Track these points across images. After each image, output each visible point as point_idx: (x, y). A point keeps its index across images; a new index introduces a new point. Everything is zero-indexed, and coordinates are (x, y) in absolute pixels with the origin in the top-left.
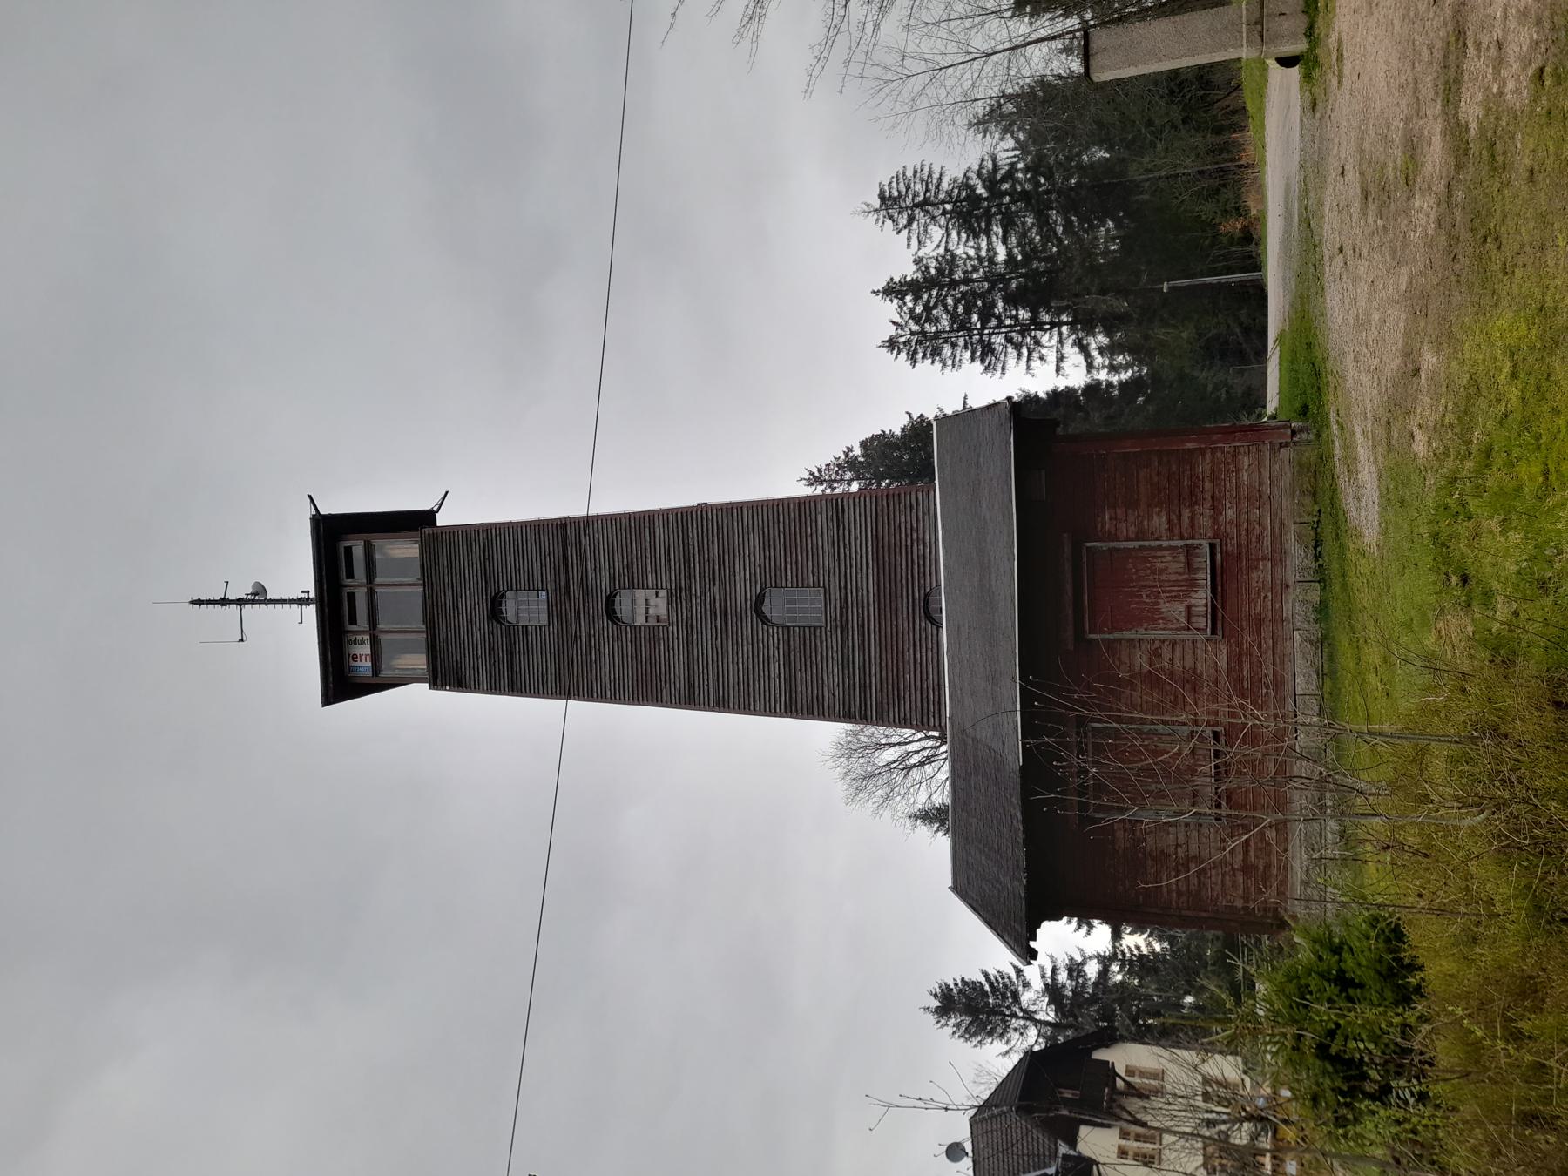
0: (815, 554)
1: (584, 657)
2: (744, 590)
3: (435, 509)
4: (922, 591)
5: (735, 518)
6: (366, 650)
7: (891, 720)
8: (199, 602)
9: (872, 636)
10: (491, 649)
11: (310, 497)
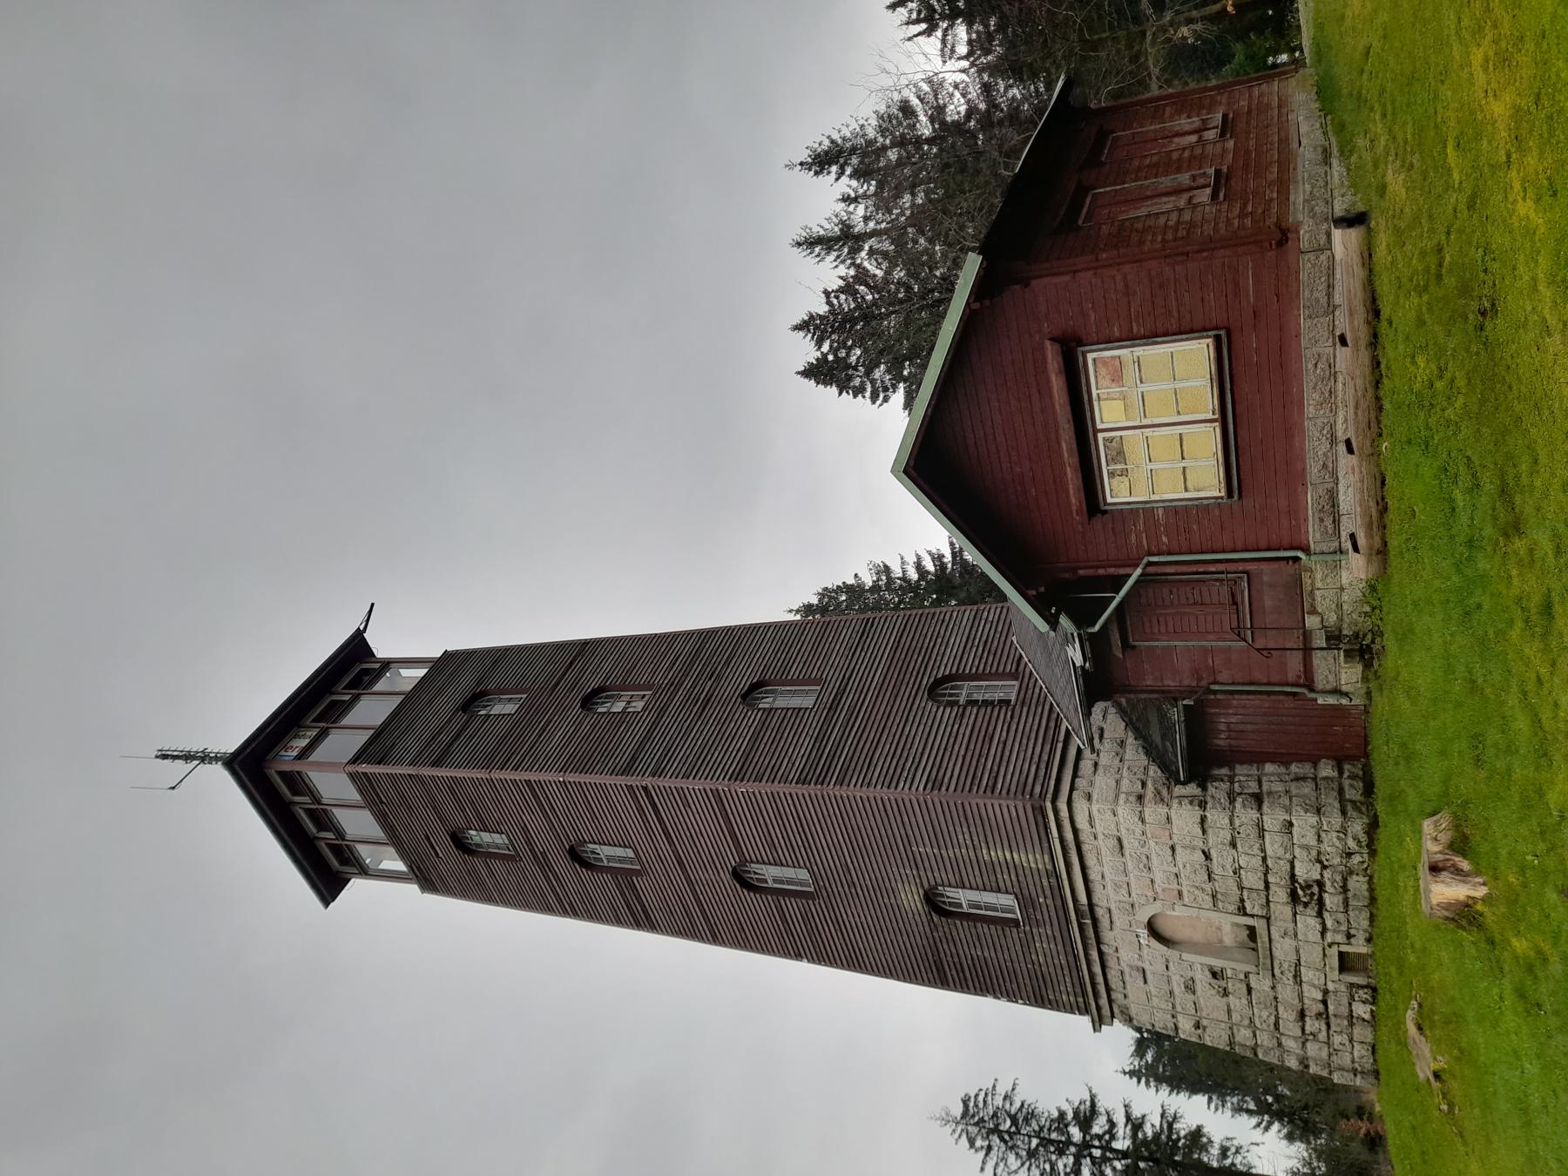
3: (362, 628)
11: (373, 605)
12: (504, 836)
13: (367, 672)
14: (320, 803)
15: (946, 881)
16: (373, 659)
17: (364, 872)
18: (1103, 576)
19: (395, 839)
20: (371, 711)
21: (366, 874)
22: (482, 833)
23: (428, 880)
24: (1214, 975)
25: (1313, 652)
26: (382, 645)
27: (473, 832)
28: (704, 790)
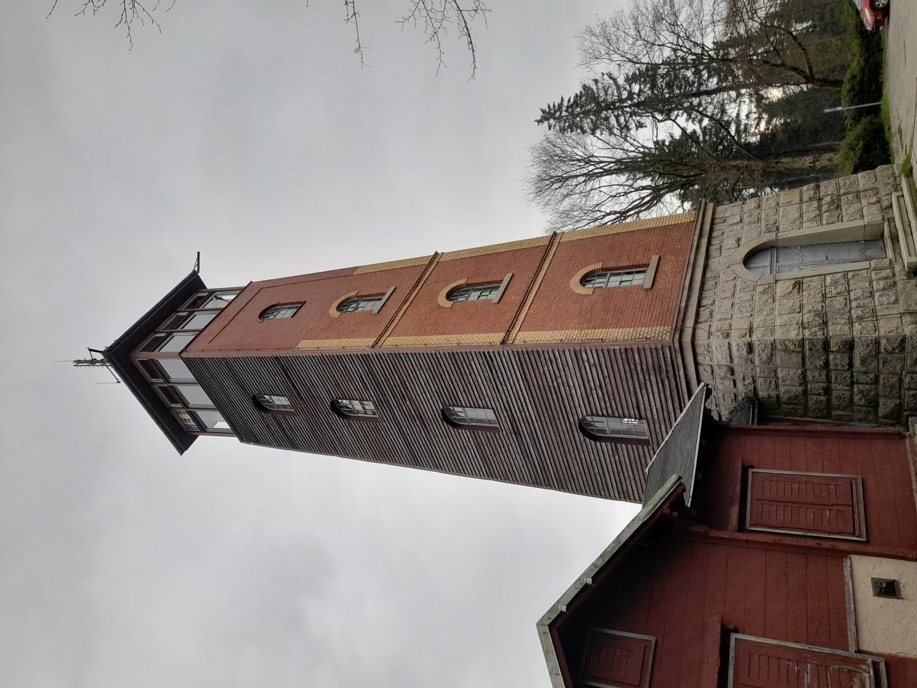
2: (431, 407)
3: (196, 269)
4: (576, 417)
5: (404, 360)
6: (187, 417)
7: (578, 488)
8: (79, 362)
9: (542, 441)
11: (199, 253)
12: (286, 397)
14: (169, 382)
16: (205, 290)
18: (848, 640)
19: (221, 406)
21: (205, 432)
23: (246, 434)
24: (843, 67)
26: (210, 283)
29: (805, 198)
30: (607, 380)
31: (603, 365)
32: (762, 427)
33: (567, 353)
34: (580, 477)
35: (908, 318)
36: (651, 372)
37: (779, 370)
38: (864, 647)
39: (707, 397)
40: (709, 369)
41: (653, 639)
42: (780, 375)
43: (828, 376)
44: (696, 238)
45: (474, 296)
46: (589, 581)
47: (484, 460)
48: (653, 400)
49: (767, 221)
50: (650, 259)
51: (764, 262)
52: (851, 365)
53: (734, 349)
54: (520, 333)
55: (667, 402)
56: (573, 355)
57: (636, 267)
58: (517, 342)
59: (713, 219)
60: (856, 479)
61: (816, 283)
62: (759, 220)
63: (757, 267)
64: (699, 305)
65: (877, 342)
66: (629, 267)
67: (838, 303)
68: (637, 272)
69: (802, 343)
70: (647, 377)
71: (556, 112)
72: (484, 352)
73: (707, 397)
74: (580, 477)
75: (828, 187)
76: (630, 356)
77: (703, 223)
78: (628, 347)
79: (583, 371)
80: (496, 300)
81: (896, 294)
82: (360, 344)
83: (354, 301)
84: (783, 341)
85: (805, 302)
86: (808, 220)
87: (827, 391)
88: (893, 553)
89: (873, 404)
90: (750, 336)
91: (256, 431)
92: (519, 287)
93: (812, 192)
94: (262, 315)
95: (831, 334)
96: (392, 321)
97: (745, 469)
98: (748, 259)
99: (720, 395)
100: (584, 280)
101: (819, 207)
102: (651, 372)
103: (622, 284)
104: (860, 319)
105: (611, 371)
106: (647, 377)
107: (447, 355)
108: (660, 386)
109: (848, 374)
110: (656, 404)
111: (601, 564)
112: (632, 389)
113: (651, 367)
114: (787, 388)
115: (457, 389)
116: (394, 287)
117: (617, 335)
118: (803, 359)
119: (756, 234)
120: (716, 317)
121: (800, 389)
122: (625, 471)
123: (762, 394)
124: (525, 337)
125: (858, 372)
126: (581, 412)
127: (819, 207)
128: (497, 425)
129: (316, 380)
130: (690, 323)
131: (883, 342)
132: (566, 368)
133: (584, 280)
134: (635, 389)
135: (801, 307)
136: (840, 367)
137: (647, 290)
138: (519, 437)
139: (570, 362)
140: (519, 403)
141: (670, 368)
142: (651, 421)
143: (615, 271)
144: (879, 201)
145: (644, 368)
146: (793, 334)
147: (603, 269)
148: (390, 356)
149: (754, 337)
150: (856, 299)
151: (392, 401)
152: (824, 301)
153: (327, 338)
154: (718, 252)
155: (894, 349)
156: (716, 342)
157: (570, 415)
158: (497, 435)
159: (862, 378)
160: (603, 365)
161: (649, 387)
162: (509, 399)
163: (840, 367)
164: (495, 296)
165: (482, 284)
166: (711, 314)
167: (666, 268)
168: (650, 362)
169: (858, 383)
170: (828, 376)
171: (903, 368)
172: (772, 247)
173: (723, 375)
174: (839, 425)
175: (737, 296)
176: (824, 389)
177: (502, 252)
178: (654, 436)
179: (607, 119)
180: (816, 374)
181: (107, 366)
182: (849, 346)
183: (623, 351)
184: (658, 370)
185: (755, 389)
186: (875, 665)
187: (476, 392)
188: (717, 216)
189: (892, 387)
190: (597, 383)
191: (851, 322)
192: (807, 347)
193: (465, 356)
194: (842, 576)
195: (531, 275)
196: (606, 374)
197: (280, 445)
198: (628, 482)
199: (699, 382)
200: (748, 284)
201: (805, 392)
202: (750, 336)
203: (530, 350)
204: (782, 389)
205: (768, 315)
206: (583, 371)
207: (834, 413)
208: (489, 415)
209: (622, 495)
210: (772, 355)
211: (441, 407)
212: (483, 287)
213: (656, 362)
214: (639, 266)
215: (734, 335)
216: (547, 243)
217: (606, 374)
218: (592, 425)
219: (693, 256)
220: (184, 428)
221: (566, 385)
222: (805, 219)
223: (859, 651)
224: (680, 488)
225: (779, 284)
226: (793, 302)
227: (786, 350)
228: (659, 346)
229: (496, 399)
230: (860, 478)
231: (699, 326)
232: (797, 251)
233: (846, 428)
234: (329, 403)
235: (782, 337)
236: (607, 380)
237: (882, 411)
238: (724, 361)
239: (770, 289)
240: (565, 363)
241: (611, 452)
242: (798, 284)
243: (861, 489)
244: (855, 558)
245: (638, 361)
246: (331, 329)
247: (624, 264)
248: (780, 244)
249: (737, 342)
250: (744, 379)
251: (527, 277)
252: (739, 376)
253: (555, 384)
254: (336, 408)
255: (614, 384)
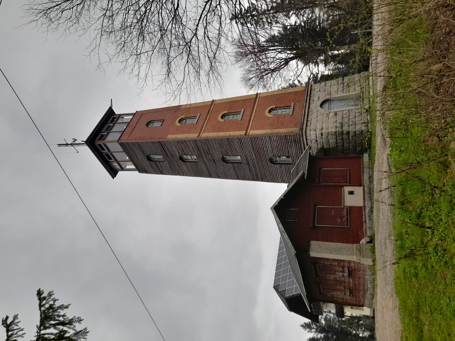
0: (236, 149)
1: (255, 160)
2: (218, 156)
3: (111, 106)
4: (268, 157)
6: (116, 164)
7: (268, 180)
8: (60, 145)
10: (152, 166)
11: (111, 99)
13: (115, 118)
15: (276, 155)
17: (123, 169)
19: (132, 160)
20: (118, 128)
21: (123, 170)
22: (155, 156)
23: (141, 169)
25: (303, 65)
26: (117, 111)
27: (152, 156)
28: (240, 138)
29: (339, 83)
30: (279, 145)
31: (278, 141)
32: (325, 157)
33: (267, 137)
34: (269, 176)
35: (363, 125)
36: (293, 142)
37: (330, 140)
38: (345, 205)
39: (310, 149)
40: (310, 140)
41: (298, 209)
42: (330, 142)
43: (343, 142)
44: (306, 97)
45: (231, 117)
46: (283, 197)
47: (236, 173)
48: (293, 151)
49: (327, 91)
50: (291, 104)
51: (326, 105)
52: (349, 138)
53: (317, 134)
54: (251, 131)
55: (297, 151)
56: (269, 138)
57: (287, 107)
58: (250, 134)
59: (311, 89)
60: (348, 169)
61: (341, 113)
62: (325, 90)
63: (324, 107)
64: (307, 121)
65: (355, 132)
66: (284, 107)
67: (346, 120)
68: (287, 108)
69: (336, 132)
70: (292, 144)
71: (238, 15)
72: (239, 138)
73: (310, 149)
74: (269, 176)
75: (346, 79)
76: (287, 137)
77: (308, 91)
78: (286, 135)
79: (272, 143)
80: (240, 119)
81: (362, 117)
82: (194, 136)
83: (184, 119)
84: (331, 132)
85: (337, 120)
86: (340, 91)
87: (343, 145)
88: (353, 185)
89: (355, 148)
90: (322, 131)
91: (146, 168)
92: (248, 113)
93: (341, 81)
94: (147, 125)
95: (344, 130)
96: (202, 127)
97: (320, 168)
98: (322, 105)
99: (313, 148)
100: (270, 112)
101: (344, 86)
102: (293, 142)
103: (283, 113)
104: (352, 125)
105: (280, 142)
106: (292, 144)
107: (226, 139)
108: (296, 146)
109: (348, 141)
110: (294, 152)
111: (285, 194)
112: (287, 147)
113: (293, 140)
114: (332, 145)
115: (228, 150)
116: (200, 114)
117: (283, 131)
118: (336, 137)
119: (324, 96)
120: (312, 124)
121: (336, 145)
122: (284, 173)
123: (325, 147)
124: (252, 132)
125: (351, 140)
126: (270, 155)
127: (344, 86)
128: (242, 161)
129: (174, 149)
130: (304, 127)
131: (357, 132)
132: (266, 142)
133: (270, 112)
134: (288, 147)
135: (336, 121)
136: (346, 139)
137: (291, 115)
138: (249, 165)
139: (268, 140)
140: (250, 154)
141: (299, 141)
142: (292, 157)
143: (280, 108)
144: (360, 85)
145: (291, 141)
146: (334, 130)
147: (276, 107)
148: (205, 140)
149: (323, 131)
150: (351, 119)
151: (204, 155)
152: (342, 119)
153: (178, 134)
154: (313, 102)
155: (360, 133)
156: (312, 133)
157: (267, 157)
158: (241, 164)
159: (352, 142)
160: (278, 141)
161: (292, 147)
162: (246, 153)
163: (346, 139)
164: (239, 117)
165: (233, 113)
166: (311, 124)
167: (297, 107)
168: (293, 138)
169: (351, 143)
170: (343, 142)
171: (362, 139)
172: (329, 100)
173: (314, 142)
174: (346, 155)
175: (318, 118)
176: (342, 145)
177: (239, 100)
178: (293, 162)
179: (262, 19)
180: (340, 141)
181: (73, 146)
182: (348, 133)
183: (284, 136)
184: (295, 141)
185: (323, 146)
186: (347, 208)
187: (235, 151)
188: (312, 88)
189: (360, 144)
190: (276, 146)
191: (349, 126)
192: (337, 133)
193: (232, 139)
194: (342, 191)
195: (251, 109)
196: (279, 143)
197: (156, 173)
198: (284, 177)
199: (307, 145)
200: (321, 113)
201: (337, 146)
202: (322, 131)
203: (255, 137)
204: (331, 146)
205: (327, 124)
206: (272, 143)
207: (345, 152)
208: (160, 157)
209: (282, 181)
210: (328, 136)
211: (222, 156)
212: (234, 114)
213: (294, 139)
214: (288, 106)
215: (317, 130)
216: (255, 97)
217: (279, 143)
218: (226, 159)
219: (305, 104)
220: (114, 169)
221: (266, 147)
222: (339, 91)
223: (344, 206)
224: (304, 174)
225: (331, 113)
226: (334, 120)
227: (332, 134)
228: (296, 134)
229: (242, 153)
230: (349, 169)
231: (307, 128)
232: (336, 101)
233: (348, 156)
234: (269, 158)
235: (331, 131)
236: (279, 145)
237: (357, 150)
238: (315, 138)
239: (328, 115)
240: (266, 140)
241: (279, 168)
242: (336, 114)
243: (349, 172)
244: (345, 187)
245: (289, 139)
246: (178, 130)
247: (283, 106)
248: (331, 99)
249: (318, 132)
250: (320, 143)
251: (249, 110)
252: (319, 142)
253: (262, 147)
254: (181, 158)
255: (281, 146)
